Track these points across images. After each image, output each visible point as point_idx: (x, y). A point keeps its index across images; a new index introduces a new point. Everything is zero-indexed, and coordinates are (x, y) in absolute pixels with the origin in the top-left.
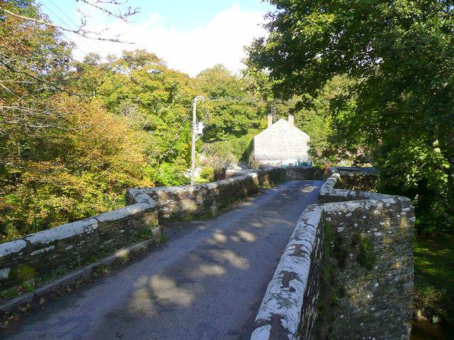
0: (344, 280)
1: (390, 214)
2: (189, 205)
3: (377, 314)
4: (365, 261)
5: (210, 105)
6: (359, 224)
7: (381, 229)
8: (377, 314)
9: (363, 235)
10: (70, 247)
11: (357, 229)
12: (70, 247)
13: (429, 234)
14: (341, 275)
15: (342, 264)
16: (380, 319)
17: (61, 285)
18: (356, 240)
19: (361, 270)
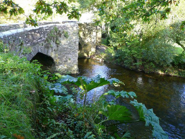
0: (61, 40)
1: (72, 27)
2: (148, 72)
3: (69, 48)
4: (66, 36)
5: (147, 93)
6: (64, 28)
7: (70, 30)
8: (69, 48)
9: (65, 31)
10: (3, 28)
11: (64, 29)
12: (3, 28)
13: (86, 45)
14: (60, 39)
15: (60, 36)
16: (70, 49)
17: (12, 36)
18: (63, 32)
19: (65, 38)
